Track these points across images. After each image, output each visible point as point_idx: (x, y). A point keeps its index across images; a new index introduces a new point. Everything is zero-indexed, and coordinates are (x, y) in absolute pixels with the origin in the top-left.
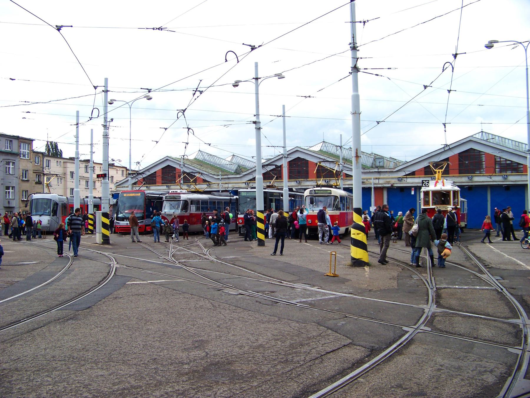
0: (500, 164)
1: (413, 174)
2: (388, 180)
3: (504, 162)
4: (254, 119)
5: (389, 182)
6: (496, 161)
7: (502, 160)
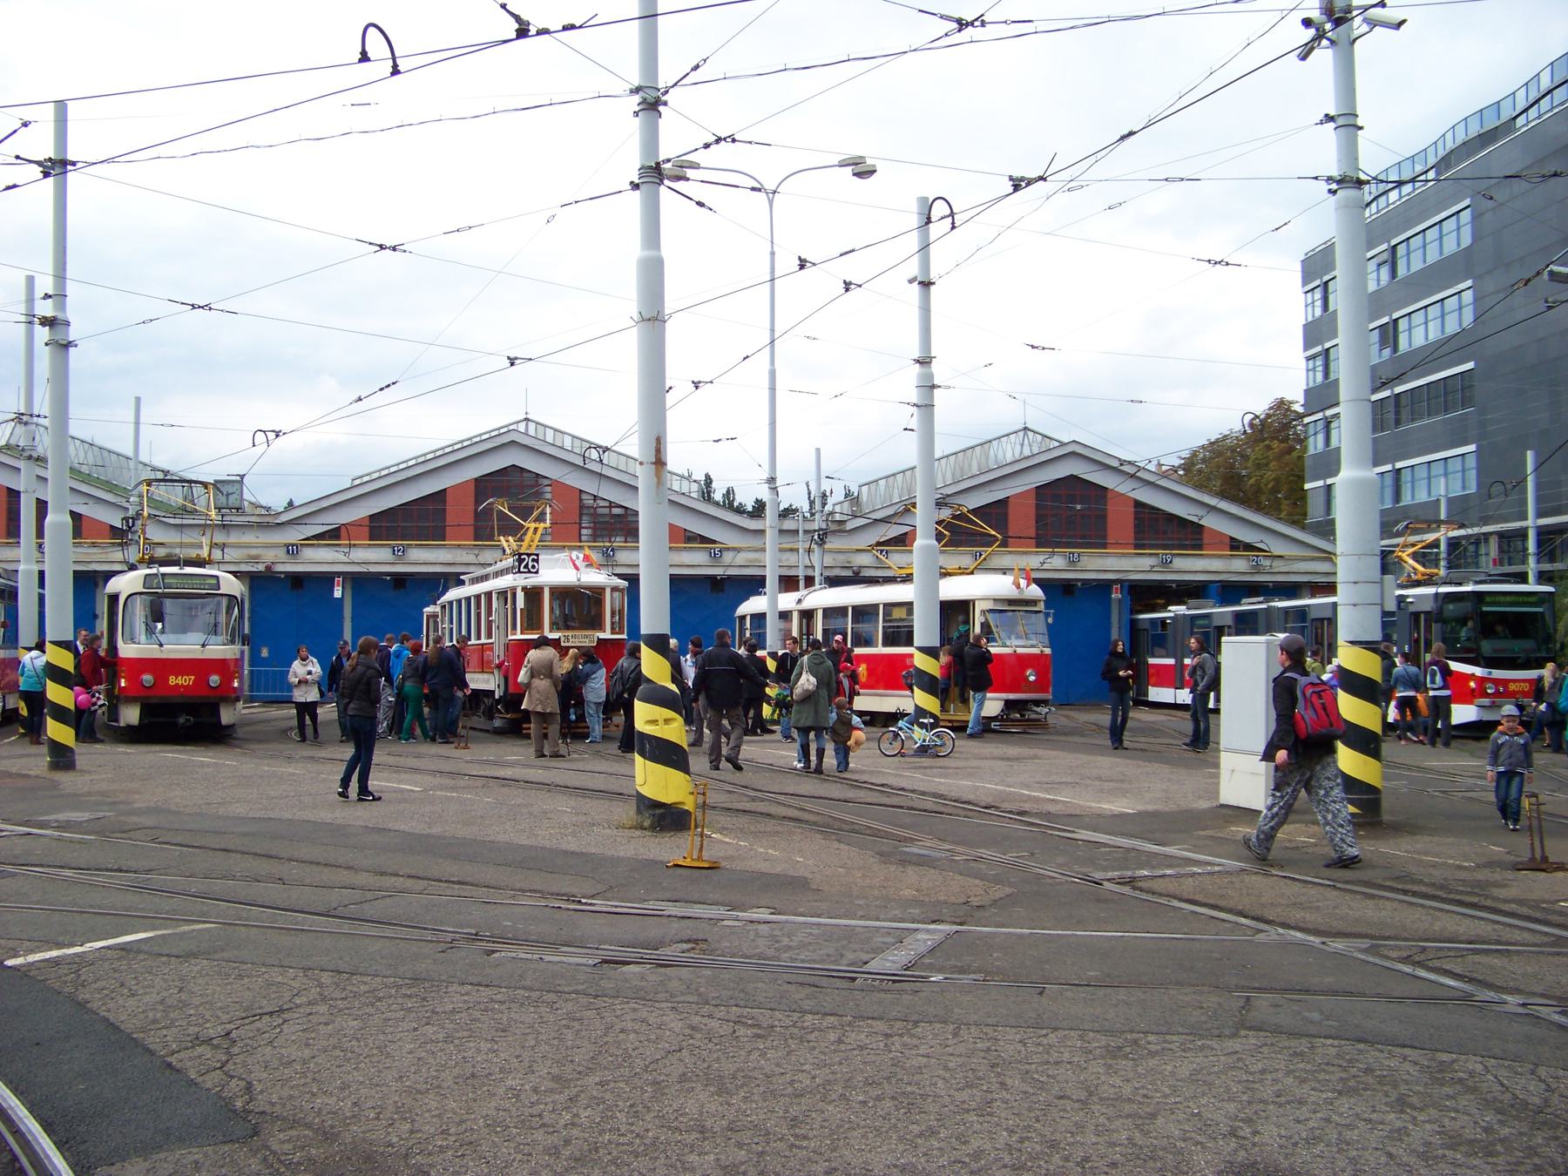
0: (595, 515)
2: (254, 552)
3: (606, 511)
5: (257, 557)
6: (582, 507)
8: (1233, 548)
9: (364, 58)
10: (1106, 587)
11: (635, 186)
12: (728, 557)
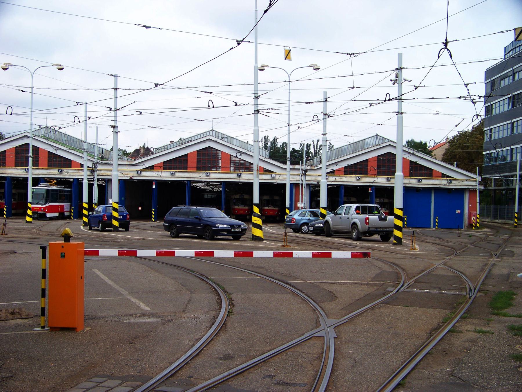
1: (152, 168)
2: (126, 173)
4: (113, 124)
6: (231, 160)
7: (236, 159)
8: (442, 177)
9: (209, 106)
10: (370, 191)
11: (253, 114)
12: (277, 177)
